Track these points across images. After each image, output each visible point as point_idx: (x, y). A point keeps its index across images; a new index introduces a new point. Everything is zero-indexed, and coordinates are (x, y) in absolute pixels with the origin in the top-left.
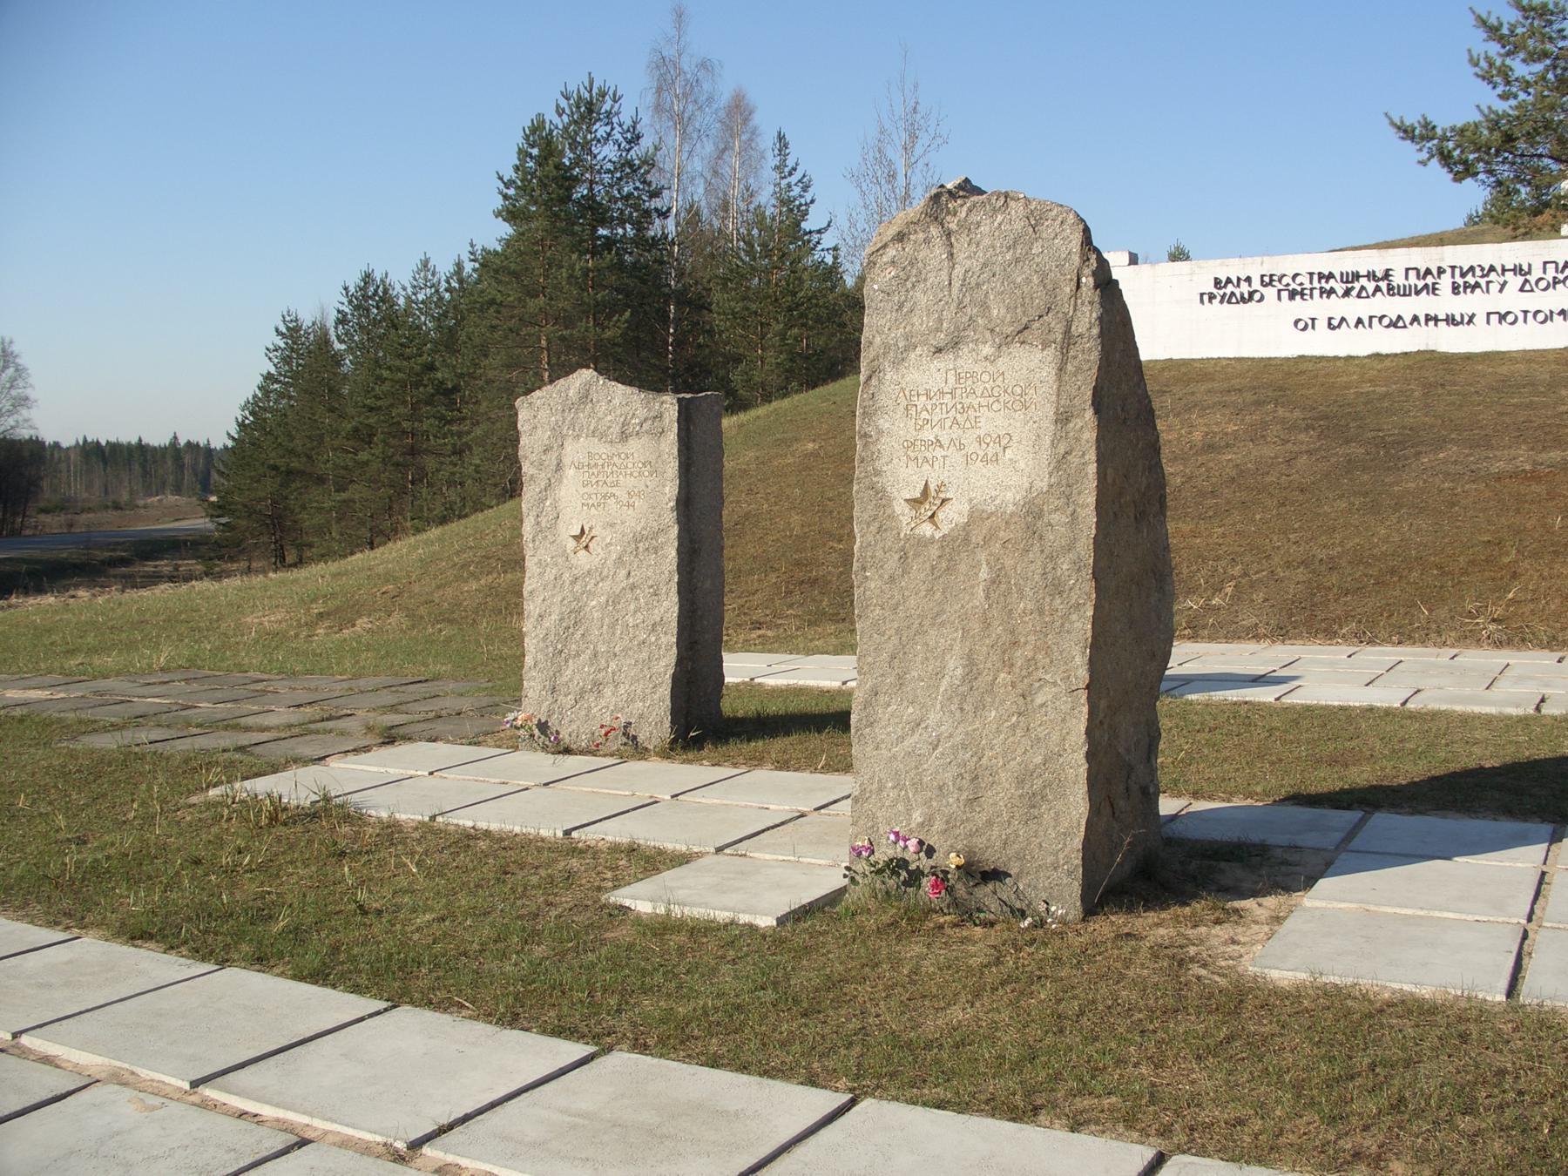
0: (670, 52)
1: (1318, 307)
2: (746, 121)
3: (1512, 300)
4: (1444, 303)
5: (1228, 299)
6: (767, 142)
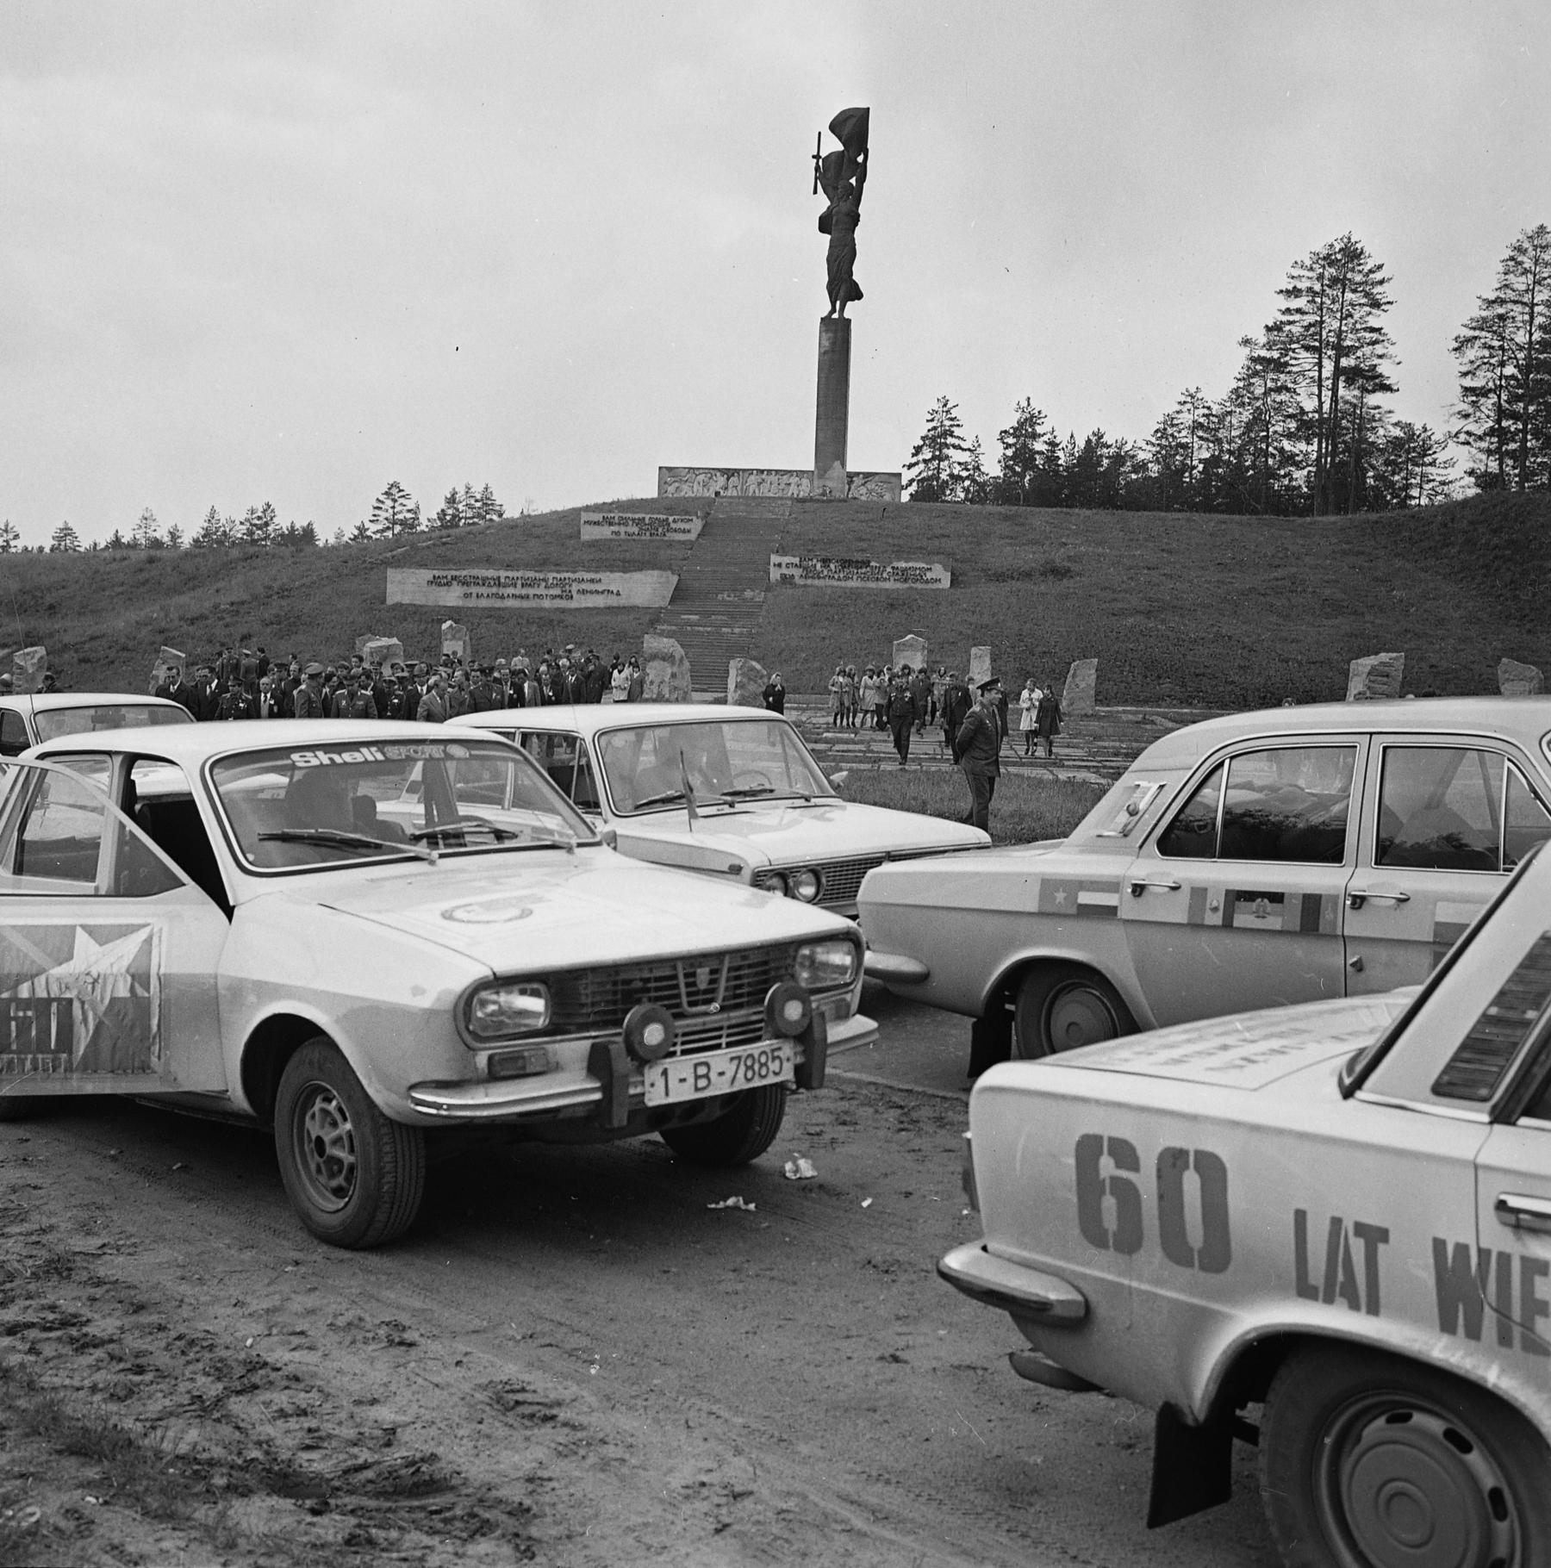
5: (440, 585)
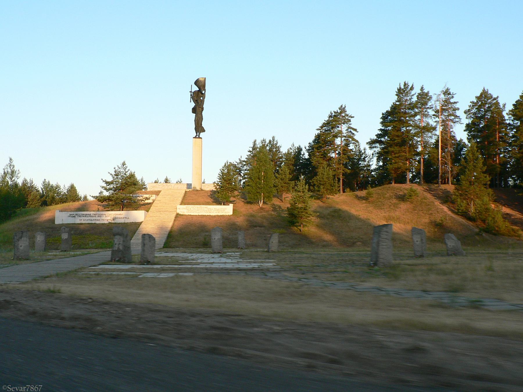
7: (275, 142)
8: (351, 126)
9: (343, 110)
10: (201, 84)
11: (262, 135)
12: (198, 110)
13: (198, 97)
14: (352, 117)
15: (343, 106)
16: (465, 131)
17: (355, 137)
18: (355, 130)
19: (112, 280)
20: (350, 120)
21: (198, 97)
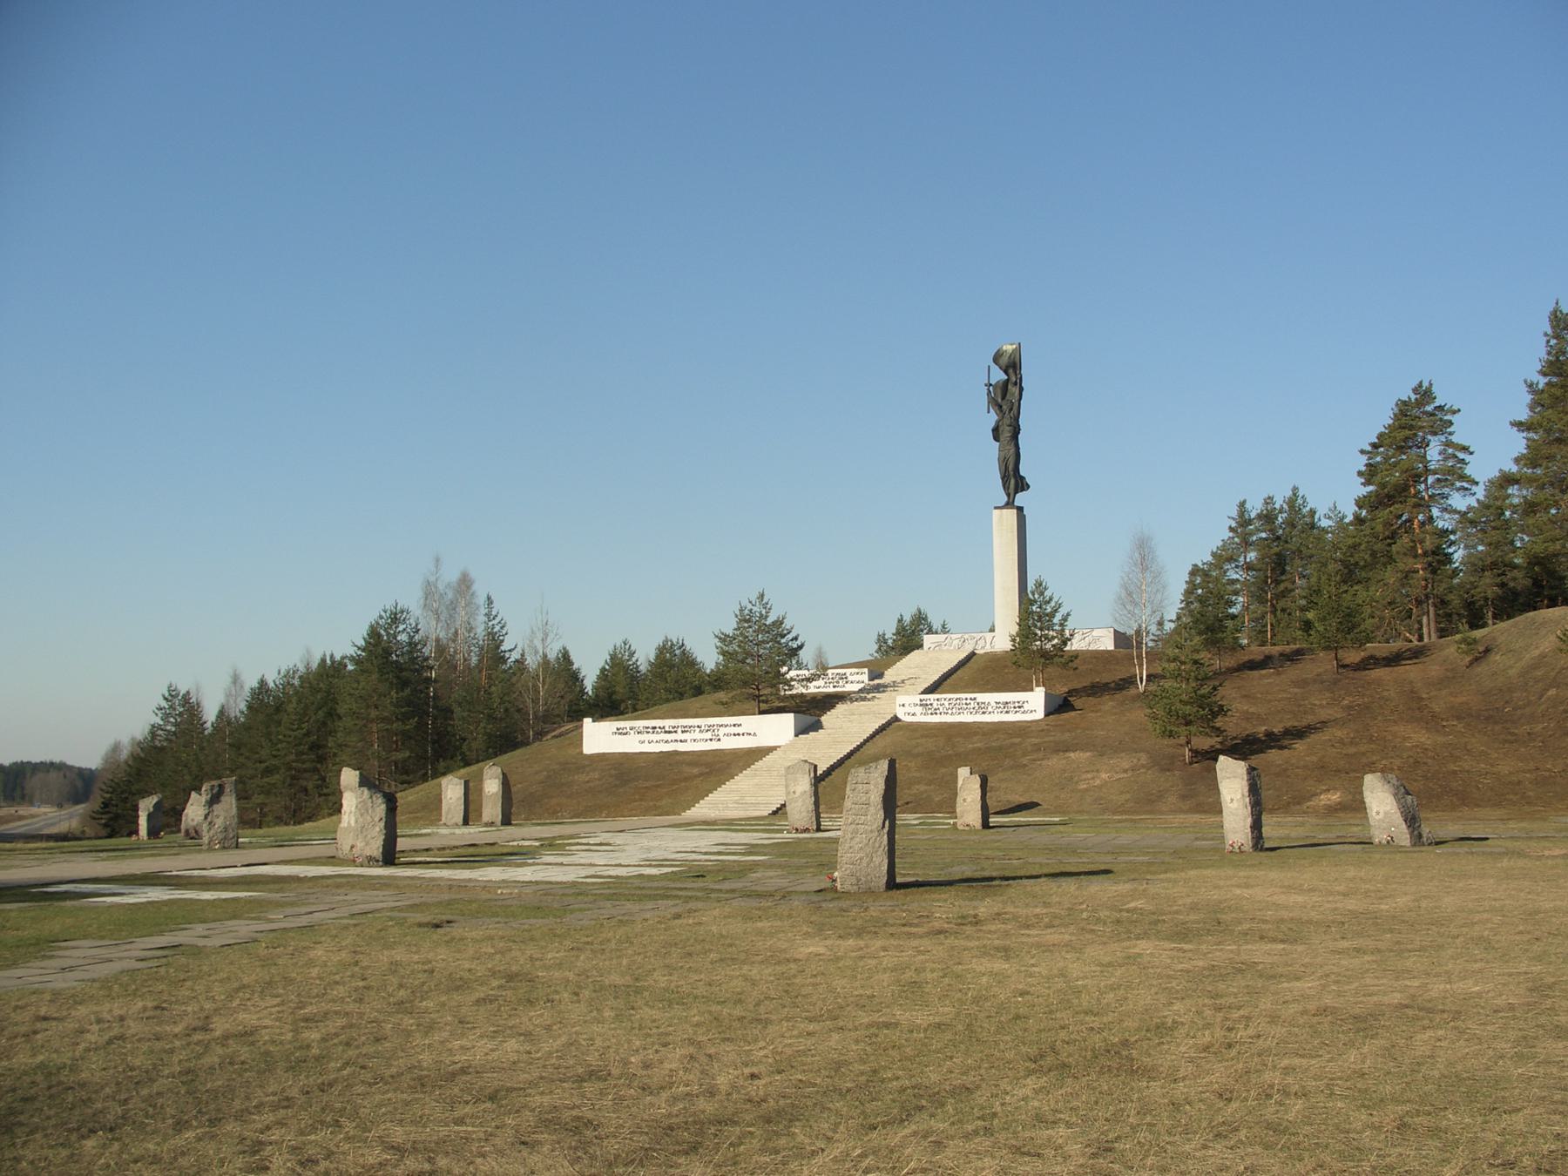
0: (432, 579)
1: (645, 737)
2: (469, 587)
3: (697, 735)
4: (680, 736)
6: (481, 600)
7: (1300, 501)
8: (1454, 439)
9: (1424, 394)
10: (1012, 366)
11: (1263, 487)
12: (1008, 431)
13: (1006, 398)
14: (1454, 412)
15: (1425, 384)
16: (1519, 425)
17: (1468, 471)
18: (1465, 449)
19: (357, 1047)
20: (1451, 423)
21: (1006, 398)
